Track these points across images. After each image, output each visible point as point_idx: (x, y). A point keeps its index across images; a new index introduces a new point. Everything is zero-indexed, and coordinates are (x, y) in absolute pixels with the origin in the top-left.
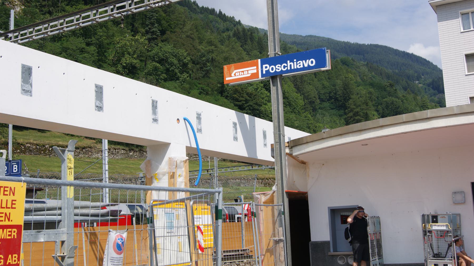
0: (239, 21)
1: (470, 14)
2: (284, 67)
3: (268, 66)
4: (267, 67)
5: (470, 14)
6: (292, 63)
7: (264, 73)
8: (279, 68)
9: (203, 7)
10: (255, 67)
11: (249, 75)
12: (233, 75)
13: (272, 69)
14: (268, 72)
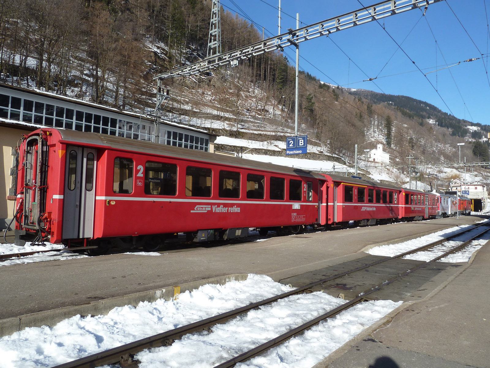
12: (195, 209)
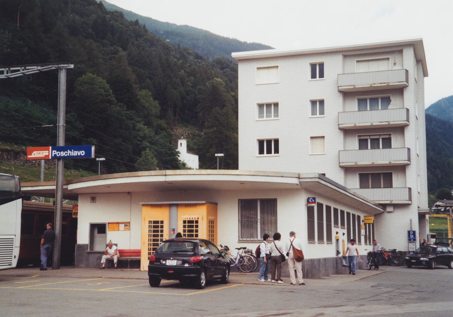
0: (101, 2)
1: (380, 100)
2: (66, 154)
3: (55, 151)
4: (55, 152)
5: (380, 100)
6: (70, 152)
7: (53, 156)
8: (63, 154)
9: (131, 21)
10: (48, 151)
11: (43, 156)
12: (33, 154)
13: (58, 154)
14: (55, 155)
